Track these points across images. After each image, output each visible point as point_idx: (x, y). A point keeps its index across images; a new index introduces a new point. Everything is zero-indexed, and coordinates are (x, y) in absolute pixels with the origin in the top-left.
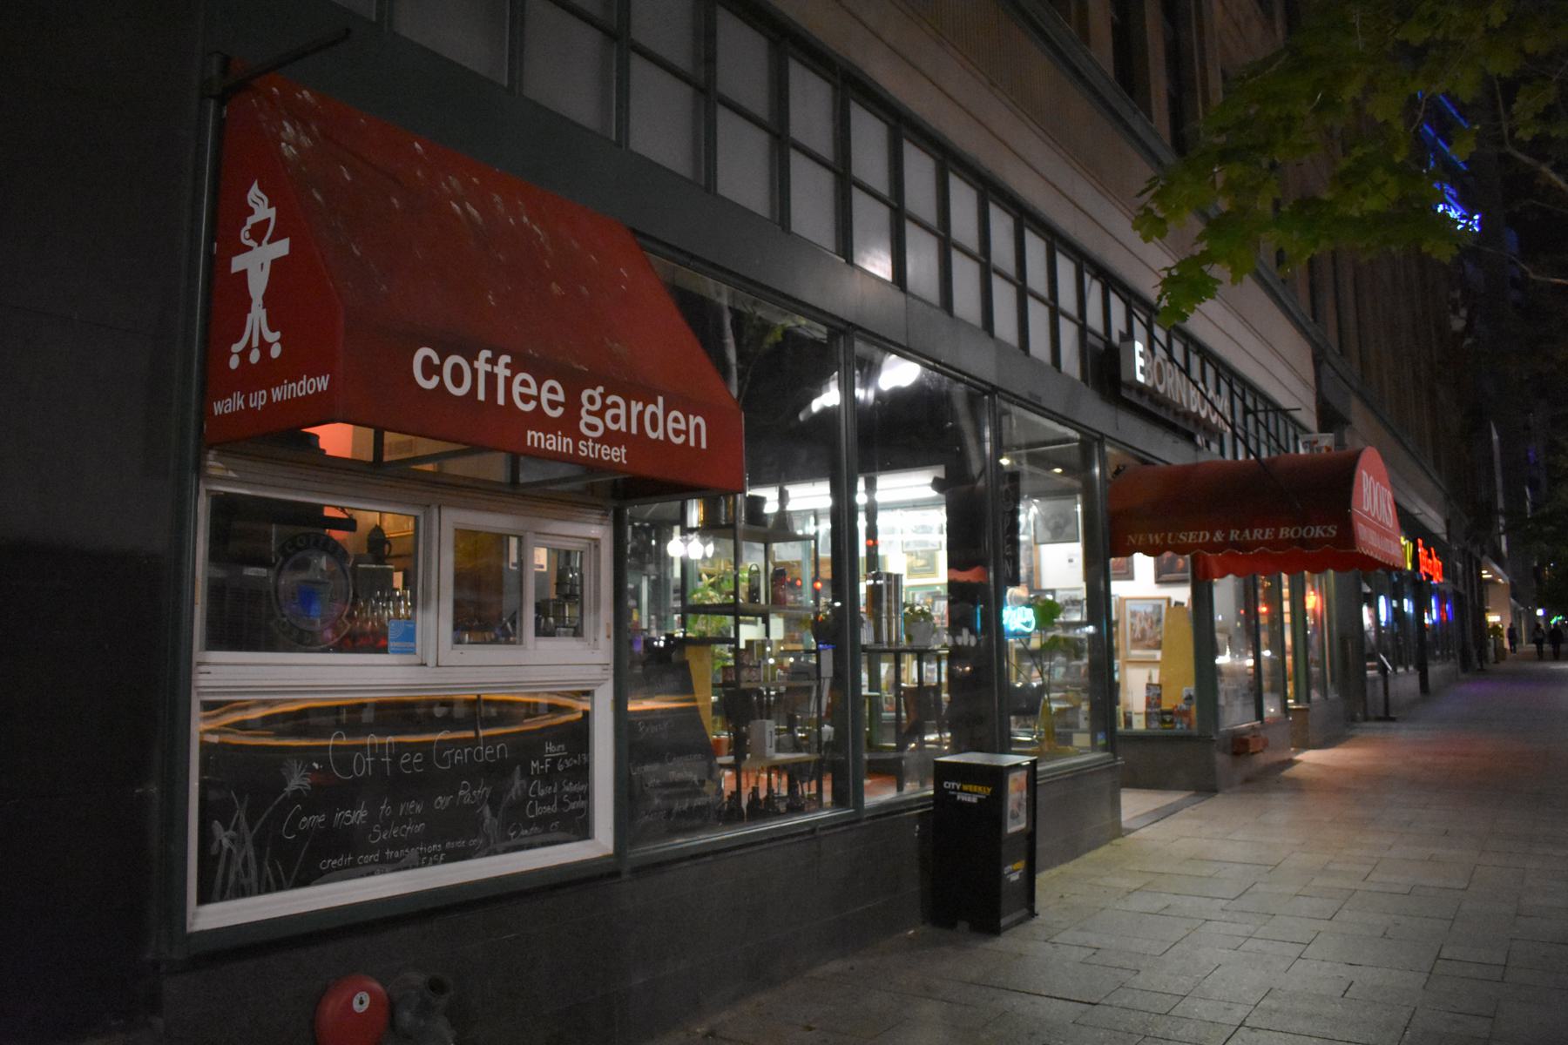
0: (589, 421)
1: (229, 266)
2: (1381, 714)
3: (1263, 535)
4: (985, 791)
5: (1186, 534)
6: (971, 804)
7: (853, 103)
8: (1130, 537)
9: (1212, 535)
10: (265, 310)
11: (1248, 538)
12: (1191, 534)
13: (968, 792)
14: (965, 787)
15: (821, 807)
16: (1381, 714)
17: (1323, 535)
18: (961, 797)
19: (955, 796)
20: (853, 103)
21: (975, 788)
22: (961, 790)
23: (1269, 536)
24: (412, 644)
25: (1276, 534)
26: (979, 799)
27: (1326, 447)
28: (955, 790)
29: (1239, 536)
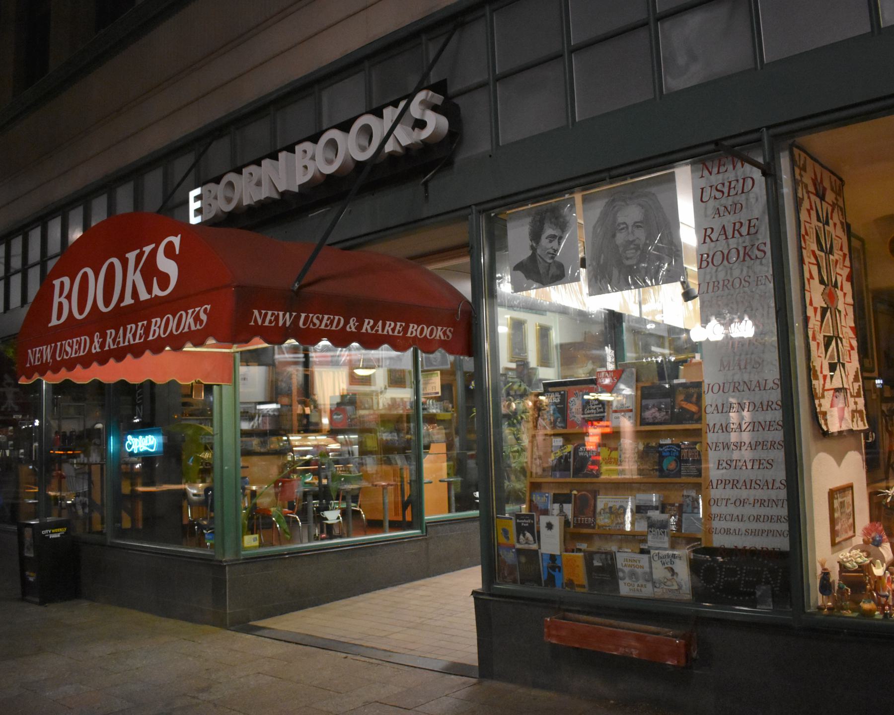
0: (58, 296)
1: (255, 309)
2: (691, 512)
3: (393, 330)
4: (62, 530)
5: (321, 316)
6: (57, 538)
7: (763, 163)
8: (256, 312)
9: (347, 322)
10: (831, 580)
11: (380, 332)
12: (326, 317)
13: (55, 533)
14: (53, 531)
15: (497, 514)
16: (691, 512)
17: (442, 338)
18: (52, 536)
19: (49, 537)
20: (763, 163)
21: (58, 530)
22: (51, 533)
23: (399, 332)
24: (453, 509)
25: (405, 329)
26: (61, 535)
27: (615, 459)
28: (49, 533)
29: (372, 328)
